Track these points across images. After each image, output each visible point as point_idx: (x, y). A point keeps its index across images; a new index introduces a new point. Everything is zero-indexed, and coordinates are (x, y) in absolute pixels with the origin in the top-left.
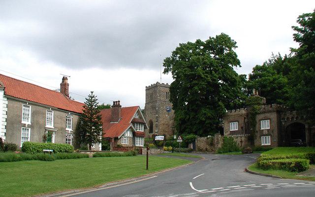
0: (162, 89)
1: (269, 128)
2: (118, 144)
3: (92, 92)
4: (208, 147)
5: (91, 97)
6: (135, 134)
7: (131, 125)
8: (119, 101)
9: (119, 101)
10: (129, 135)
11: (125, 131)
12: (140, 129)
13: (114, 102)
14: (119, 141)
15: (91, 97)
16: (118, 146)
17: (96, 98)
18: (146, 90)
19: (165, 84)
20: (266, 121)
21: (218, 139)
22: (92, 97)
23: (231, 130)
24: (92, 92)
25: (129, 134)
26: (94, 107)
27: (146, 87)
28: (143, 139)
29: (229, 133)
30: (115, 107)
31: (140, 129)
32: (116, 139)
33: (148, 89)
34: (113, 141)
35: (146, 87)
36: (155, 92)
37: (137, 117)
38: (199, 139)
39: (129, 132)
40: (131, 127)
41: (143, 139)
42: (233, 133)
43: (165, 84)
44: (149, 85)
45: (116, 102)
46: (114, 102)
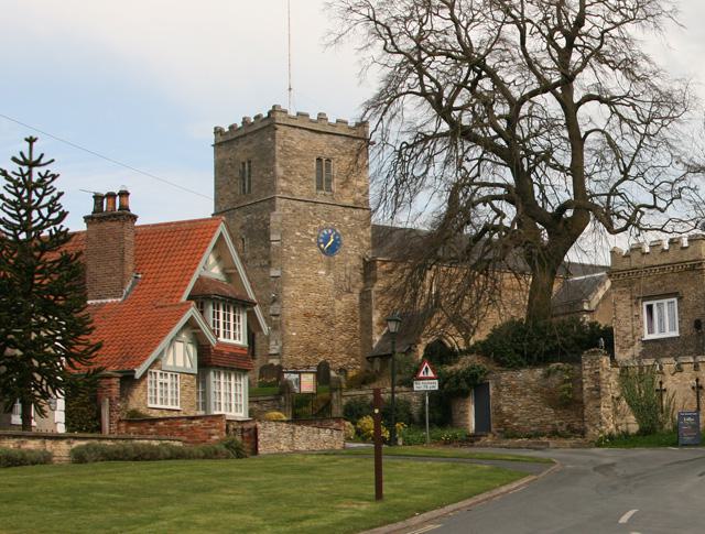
0: (298, 141)
1: (676, 334)
2: (133, 405)
3: (31, 141)
4: (550, 416)
5: (25, 163)
6: (210, 360)
7: (192, 311)
8: (124, 194)
9: (124, 194)
10: (180, 363)
11: (165, 343)
12: (232, 334)
13: (98, 198)
14: (137, 392)
15: (25, 163)
16: (135, 413)
17: (53, 169)
18: (217, 145)
19: (314, 117)
20: (665, 301)
21: (596, 378)
22: (32, 164)
23: (648, 337)
24: (31, 141)
25: (181, 356)
26: (45, 212)
27: (218, 131)
28: (244, 381)
29: (637, 349)
30: (107, 225)
31: (232, 334)
32: (129, 381)
33: (226, 141)
34: (115, 390)
35: (218, 131)
36: (267, 156)
37: (215, 272)
38: (505, 376)
39: (179, 347)
40: (191, 324)
41: (244, 381)
42: (657, 348)
43: (314, 117)
44: (231, 118)
45: (111, 196)
46: (98, 198)
